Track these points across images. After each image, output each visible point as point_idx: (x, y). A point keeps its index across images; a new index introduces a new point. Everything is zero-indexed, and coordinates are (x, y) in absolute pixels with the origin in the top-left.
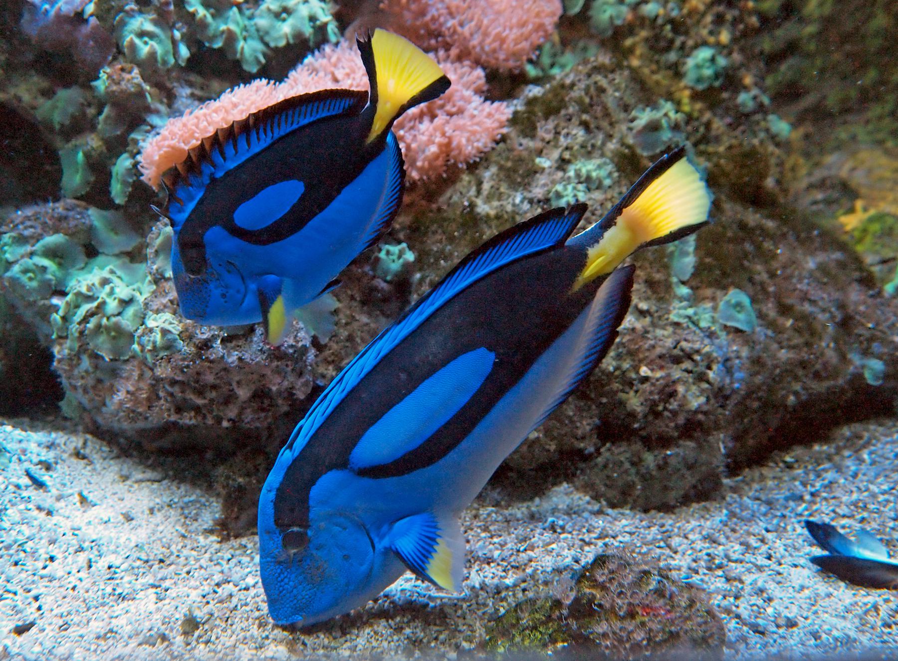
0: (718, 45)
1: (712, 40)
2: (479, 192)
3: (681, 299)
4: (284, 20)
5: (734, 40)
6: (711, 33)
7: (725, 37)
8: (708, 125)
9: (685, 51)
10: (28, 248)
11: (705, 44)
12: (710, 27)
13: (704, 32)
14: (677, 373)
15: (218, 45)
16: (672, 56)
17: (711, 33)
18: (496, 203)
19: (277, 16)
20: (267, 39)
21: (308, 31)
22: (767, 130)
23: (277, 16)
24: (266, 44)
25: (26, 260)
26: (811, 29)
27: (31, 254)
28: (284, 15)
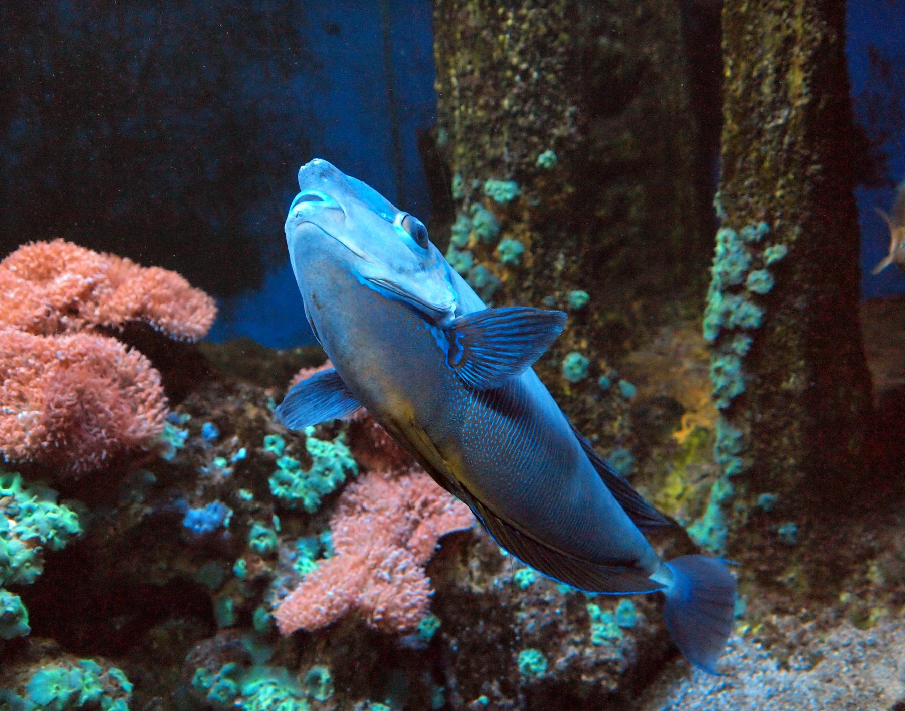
0: (581, 351)
1: (576, 347)
2: (472, 578)
3: (591, 438)
4: (327, 476)
5: (590, 345)
6: (576, 342)
7: (584, 344)
8: (584, 402)
9: (561, 357)
10: (216, 676)
11: (572, 350)
12: (575, 339)
13: (571, 342)
14: (601, 675)
15: (294, 506)
16: (553, 362)
17: (576, 342)
18: (483, 585)
19: (323, 474)
20: (320, 489)
21: (343, 477)
22: (621, 396)
23: (323, 474)
24: (320, 493)
25: (217, 684)
26: (635, 229)
27: (218, 680)
28: (327, 473)
